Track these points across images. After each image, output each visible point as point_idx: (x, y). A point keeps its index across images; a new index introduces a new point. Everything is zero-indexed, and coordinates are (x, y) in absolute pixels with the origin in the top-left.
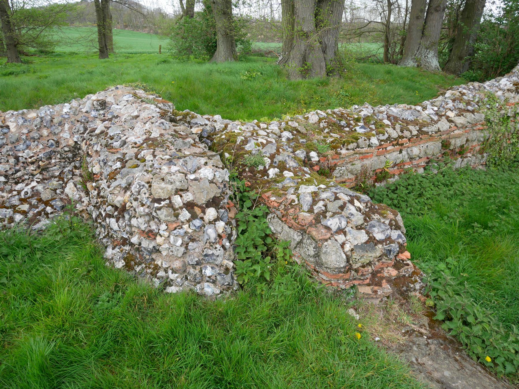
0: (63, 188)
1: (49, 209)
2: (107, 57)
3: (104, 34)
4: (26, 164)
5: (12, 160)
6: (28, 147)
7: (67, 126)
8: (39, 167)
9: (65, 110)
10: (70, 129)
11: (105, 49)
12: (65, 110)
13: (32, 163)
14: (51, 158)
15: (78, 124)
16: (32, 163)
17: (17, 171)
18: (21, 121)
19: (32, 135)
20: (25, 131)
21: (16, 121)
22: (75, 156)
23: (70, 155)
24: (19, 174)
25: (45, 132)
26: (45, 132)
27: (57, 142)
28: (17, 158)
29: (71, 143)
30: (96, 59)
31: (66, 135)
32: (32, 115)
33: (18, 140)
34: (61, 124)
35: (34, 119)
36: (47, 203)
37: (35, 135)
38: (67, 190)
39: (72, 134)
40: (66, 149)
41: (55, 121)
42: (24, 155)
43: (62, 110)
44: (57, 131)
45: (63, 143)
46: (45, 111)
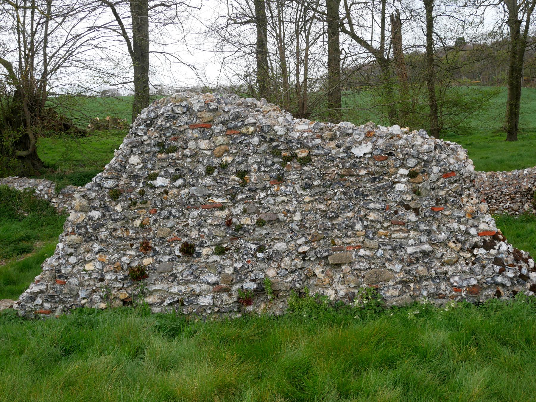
0: (523, 207)
1: (517, 213)
2: (516, 140)
3: (515, 114)
4: (505, 195)
5: (500, 193)
6: (507, 188)
7: (525, 180)
8: (510, 197)
9: (525, 172)
10: (527, 181)
11: (514, 130)
12: (525, 172)
13: (508, 195)
14: (516, 194)
15: (531, 179)
16: (508, 195)
17: (501, 198)
18: (505, 176)
19: (509, 182)
20: (507, 180)
21: (502, 176)
22: (527, 194)
23: (525, 193)
24: (501, 200)
25: (515, 182)
26: (515, 182)
27: (520, 187)
28: (502, 192)
29: (527, 187)
30: (502, 142)
31: (525, 184)
32: (509, 173)
33: (503, 184)
34: (523, 178)
35: (510, 175)
36: (516, 211)
37: (511, 183)
38: (525, 207)
39: (528, 184)
40: (524, 190)
41: (520, 177)
42: (505, 191)
43: (523, 172)
44: (520, 182)
45: (522, 187)
46: (516, 172)
